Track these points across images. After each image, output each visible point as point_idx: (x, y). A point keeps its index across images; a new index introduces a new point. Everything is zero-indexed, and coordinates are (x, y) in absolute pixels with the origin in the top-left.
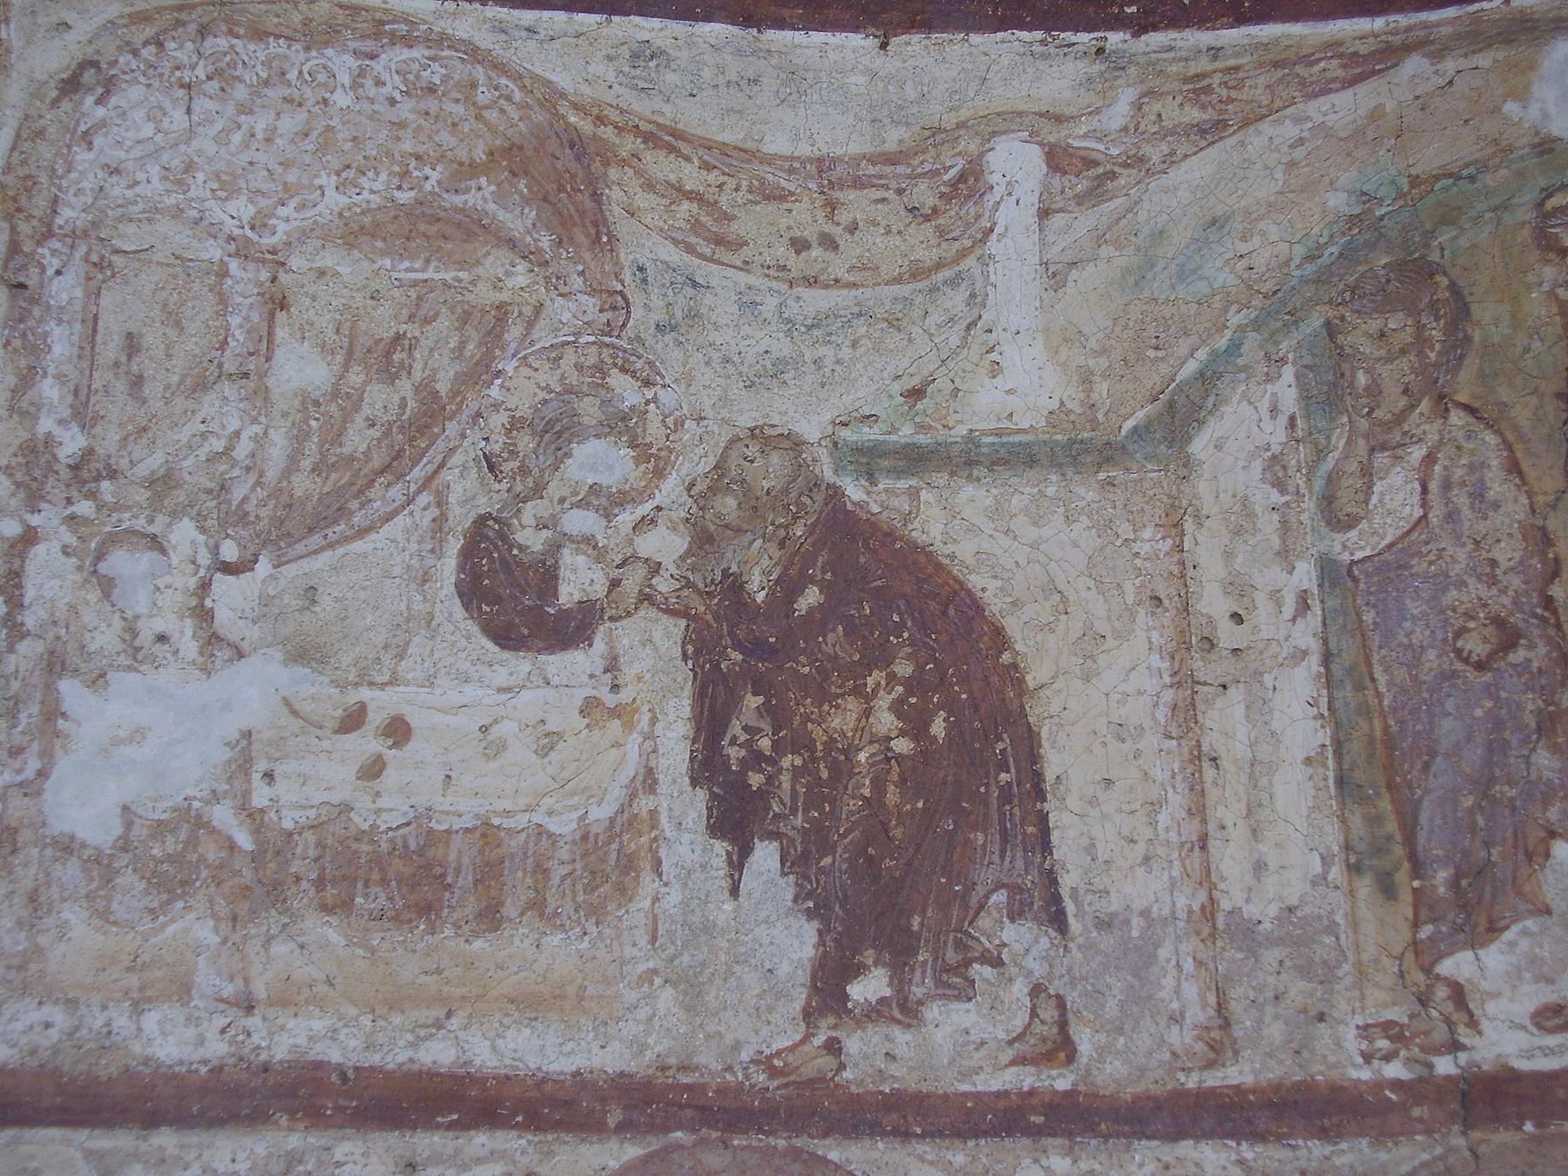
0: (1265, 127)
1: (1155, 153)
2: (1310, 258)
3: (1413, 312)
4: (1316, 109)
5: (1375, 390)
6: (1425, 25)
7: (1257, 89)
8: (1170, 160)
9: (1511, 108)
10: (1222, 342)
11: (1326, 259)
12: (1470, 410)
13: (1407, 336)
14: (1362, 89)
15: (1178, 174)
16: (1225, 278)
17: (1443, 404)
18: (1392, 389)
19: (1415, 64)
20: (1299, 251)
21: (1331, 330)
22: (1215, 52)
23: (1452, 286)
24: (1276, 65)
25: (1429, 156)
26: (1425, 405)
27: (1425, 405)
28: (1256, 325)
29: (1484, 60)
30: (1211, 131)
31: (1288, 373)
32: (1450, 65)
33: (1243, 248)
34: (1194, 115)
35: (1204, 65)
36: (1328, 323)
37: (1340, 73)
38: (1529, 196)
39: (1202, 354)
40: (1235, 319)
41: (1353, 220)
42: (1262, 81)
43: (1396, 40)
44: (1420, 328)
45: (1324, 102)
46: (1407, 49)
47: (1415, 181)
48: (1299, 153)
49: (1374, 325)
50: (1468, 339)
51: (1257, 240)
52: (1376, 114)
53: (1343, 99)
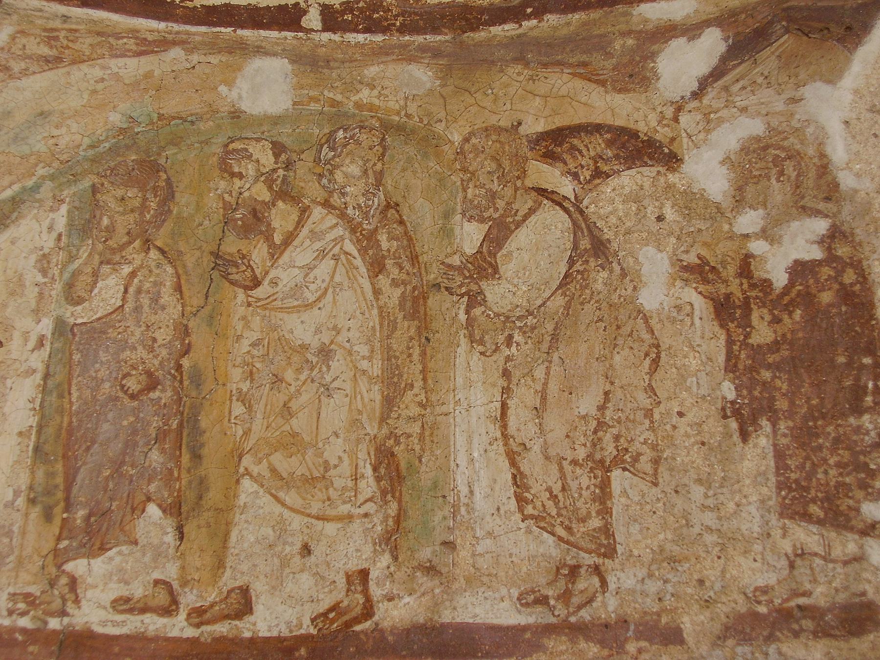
0: (84, 67)
1: (17, 66)
2: (92, 147)
3: (143, 189)
4: (116, 64)
5: (111, 230)
6: (188, 33)
7: (84, 45)
8: (25, 73)
9: (223, 89)
10: (30, 183)
11: (101, 149)
12: (162, 252)
13: (137, 203)
14: (143, 59)
15: (25, 82)
16: (41, 147)
17: (147, 244)
18: (121, 230)
19: (176, 53)
20: (87, 141)
21: (94, 189)
22: (65, 18)
23: (168, 181)
24: (99, 34)
25: (172, 105)
26: (137, 243)
27: (137, 243)
28: (52, 178)
29: (214, 59)
30: (52, 62)
31: (64, 209)
32: (195, 58)
33: (55, 132)
34: (45, 50)
35: (57, 24)
36: (93, 186)
37: (134, 48)
38: (221, 140)
39: (16, 187)
40: (41, 171)
41: (122, 131)
42: (89, 41)
43: (170, 37)
44: (145, 199)
45: (121, 61)
46: (174, 43)
47: (161, 117)
48: (100, 86)
49: (120, 193)
50: (170, 211)
51: (64, 130)
52: (148, 75)
53: (132, 63)
